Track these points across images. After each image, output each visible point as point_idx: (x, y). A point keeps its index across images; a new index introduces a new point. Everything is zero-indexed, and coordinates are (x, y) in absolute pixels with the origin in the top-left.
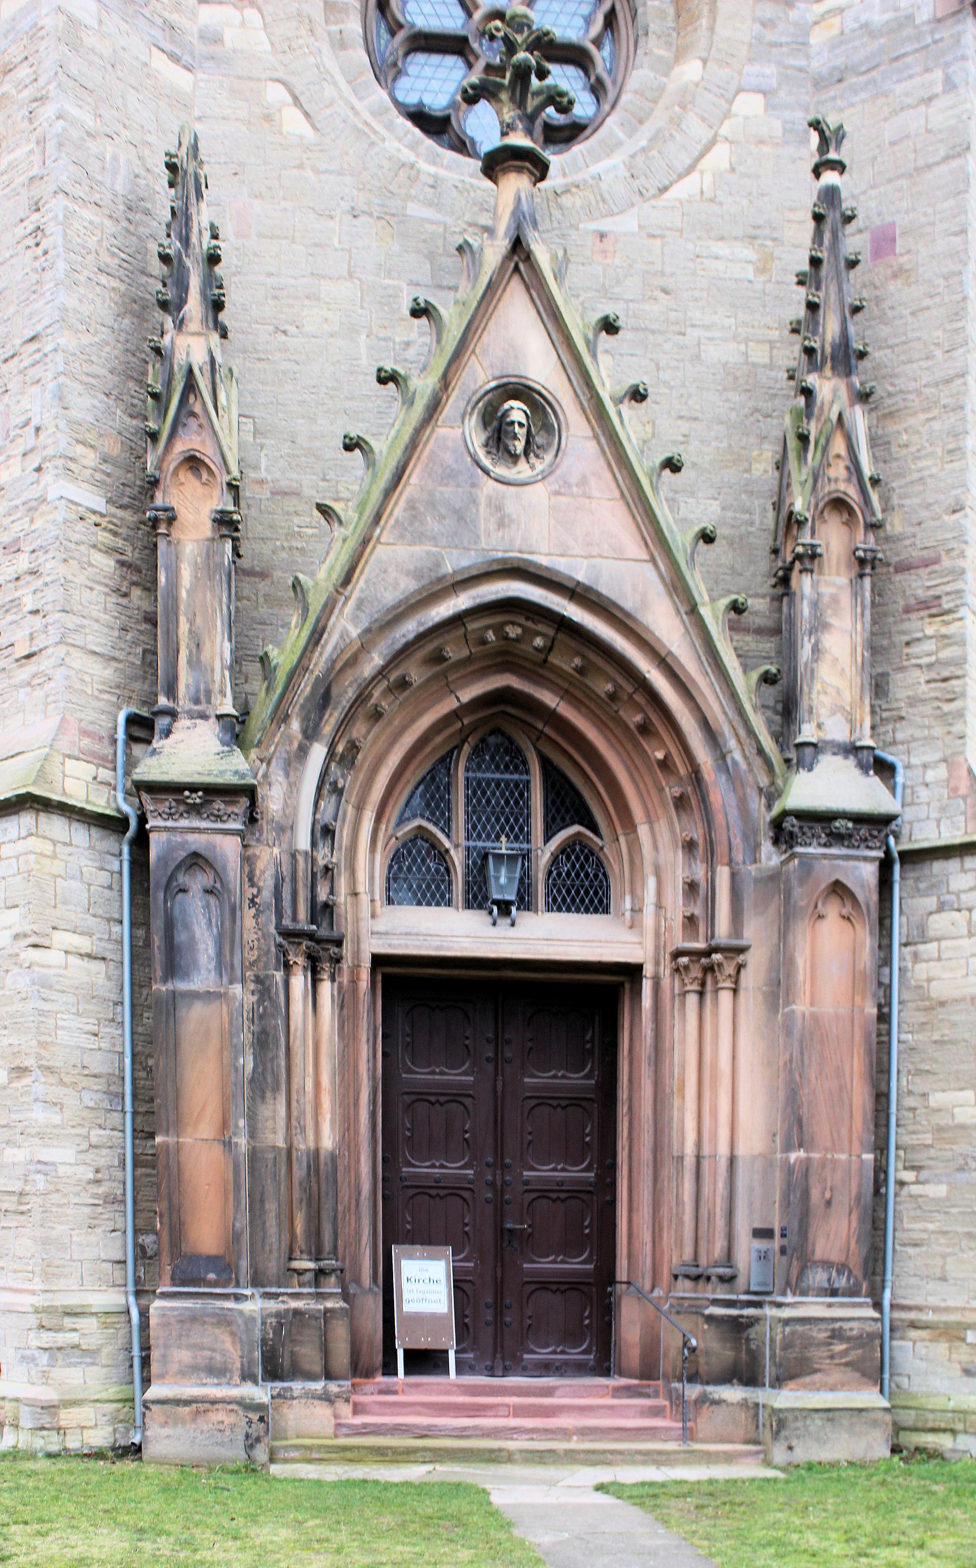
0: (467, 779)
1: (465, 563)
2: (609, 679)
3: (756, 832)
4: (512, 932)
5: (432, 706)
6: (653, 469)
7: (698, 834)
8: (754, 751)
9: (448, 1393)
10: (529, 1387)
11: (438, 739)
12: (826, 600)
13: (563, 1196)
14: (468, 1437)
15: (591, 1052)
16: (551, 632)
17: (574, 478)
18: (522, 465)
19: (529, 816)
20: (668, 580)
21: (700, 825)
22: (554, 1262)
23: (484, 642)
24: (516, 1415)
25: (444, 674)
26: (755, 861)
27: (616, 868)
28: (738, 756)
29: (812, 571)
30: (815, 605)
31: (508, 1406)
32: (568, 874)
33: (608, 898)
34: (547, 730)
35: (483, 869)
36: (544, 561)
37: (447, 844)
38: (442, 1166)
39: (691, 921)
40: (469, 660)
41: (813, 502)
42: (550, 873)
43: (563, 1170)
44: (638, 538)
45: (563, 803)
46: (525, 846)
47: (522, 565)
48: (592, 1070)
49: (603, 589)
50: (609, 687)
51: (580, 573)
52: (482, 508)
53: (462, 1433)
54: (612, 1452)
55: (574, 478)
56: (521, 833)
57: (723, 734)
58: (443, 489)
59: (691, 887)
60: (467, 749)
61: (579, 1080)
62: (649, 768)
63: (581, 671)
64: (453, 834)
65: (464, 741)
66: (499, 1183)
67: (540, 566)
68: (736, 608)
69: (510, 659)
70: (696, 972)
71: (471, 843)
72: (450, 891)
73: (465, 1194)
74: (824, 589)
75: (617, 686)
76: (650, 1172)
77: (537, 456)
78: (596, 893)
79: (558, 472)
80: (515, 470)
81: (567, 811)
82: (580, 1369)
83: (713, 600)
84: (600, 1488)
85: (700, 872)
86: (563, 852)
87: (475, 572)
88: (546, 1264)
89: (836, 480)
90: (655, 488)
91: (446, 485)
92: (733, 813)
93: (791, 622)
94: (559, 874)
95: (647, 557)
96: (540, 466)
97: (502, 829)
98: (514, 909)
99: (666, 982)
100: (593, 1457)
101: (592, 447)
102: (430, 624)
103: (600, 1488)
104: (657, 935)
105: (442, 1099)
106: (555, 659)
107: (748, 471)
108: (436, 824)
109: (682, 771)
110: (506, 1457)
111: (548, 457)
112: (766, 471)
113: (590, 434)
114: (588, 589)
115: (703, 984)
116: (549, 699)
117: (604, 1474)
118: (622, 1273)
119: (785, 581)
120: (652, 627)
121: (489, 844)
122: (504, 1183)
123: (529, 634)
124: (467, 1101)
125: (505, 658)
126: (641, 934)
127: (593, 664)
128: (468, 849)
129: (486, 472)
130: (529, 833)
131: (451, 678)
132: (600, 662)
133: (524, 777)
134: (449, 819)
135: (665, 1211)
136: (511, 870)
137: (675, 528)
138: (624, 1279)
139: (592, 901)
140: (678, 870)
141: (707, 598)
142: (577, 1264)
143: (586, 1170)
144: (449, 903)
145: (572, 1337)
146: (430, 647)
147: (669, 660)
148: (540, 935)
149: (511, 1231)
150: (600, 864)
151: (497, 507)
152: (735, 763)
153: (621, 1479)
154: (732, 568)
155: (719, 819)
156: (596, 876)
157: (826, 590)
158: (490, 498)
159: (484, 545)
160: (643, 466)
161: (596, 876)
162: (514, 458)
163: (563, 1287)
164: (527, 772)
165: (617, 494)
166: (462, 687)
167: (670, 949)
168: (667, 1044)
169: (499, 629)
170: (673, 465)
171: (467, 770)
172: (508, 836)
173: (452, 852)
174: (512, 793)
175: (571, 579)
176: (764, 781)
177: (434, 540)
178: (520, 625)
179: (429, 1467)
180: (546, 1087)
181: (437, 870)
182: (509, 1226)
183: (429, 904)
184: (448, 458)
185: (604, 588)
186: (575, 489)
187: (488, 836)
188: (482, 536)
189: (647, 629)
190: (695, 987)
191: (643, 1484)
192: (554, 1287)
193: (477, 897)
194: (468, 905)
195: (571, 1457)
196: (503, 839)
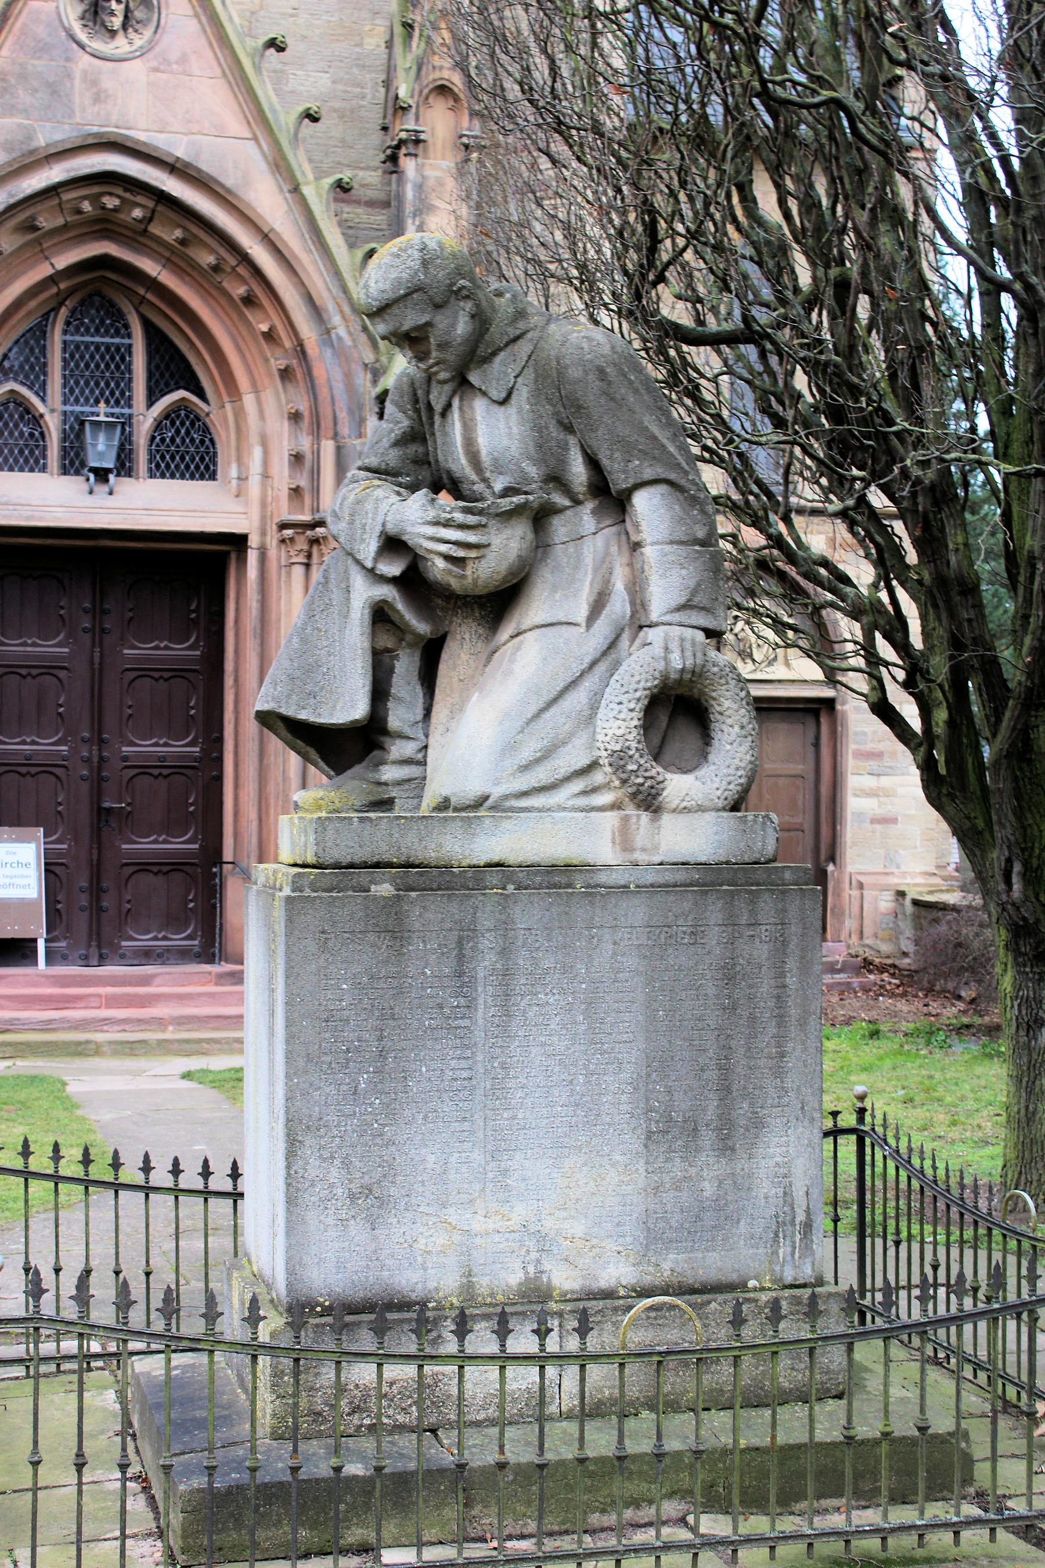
0: (65, 342)
1: (58, 137)
2: (212, 251)
3: (361, 407)
4: (110, 502)
5: (24, 273)
6: (255, 49)
7: (303, 406)
8: (360, 328)
9: (35, 985)
10: (124, 977)
11: (33, 304)
12: (431, 183)
13: (165, 772)
14: (54, 1030)
15: (195, 622)
16: (151, 204)
17: (174, 56)
18: (121, 40)
19: (130, 380)
20: (270, 158)
21: (306, 397)
22: (155, 842)
23: (79, 212)
24: (108, 1006)
25: (38, 242)
26: (360, 435)
27: (223, 433)
28: (342, 332)
29: (416, 155)
30: (420, 187)
31: (99, 996)
32: (173, 440)
33: (215, 464)
34: (149, 296)
35: (80, 435)
36: (142, 136)
37: (41, 408)
38: (34, 743)
39: (296, 492)
40: (65, 227)
41: (417, 88)
42: (153, 438)
43: (166, 745)
44: (241, 116)
45: (167, 367)
46: (126, 411)
47: (119, 140)
48: (197, 640)
49: (204, 167)
50: (211, 259)
51: (180, 149)
52: (77, 83)
53: (47, 1026)
54: (208, 1041)
55: (174, 56)
56: (122, 397)
57: (327, 311)
58: (35, 62)
59: (297, 458)
60: (63, 312)
61: (184, 651)
62: (256, 340)
63: (183, 242)
64: (49, 398)
65: (61, 304)
66: (96, 759)
67: (138, 142)
68: (342, 188)
69: (109, 226)
70: (302, 544)
71: (68, 408)
72: (45, 457)
73: (58, 771)
74: (429, 172)
75: (220, 258)
76: (256, 747)
77: (136, 31)
78: (202, 459)
79: (157, 49)
80: (113, 45)
81: (172, 376)
82: (184, 955)
83: (317, 179)
84: (187, 1076)
85: (305, 444)
86: (166, 418)
87: (69, 146)
88: (146, 845)
89: (441, 68)
90: (258, 68)
91: (39, 58)
92: (339, 388)
93: (400, 198)
94: (163, 440)
95: (249, 136)
96: (139, 41)
97: (102, 394)
98: (111, 477)
99: (273, 552)
100: (188, 1046)
101: (193, 26)
102: (21, 196)
103: (187, 1076)
104: (264, 505)
105: (34, 672)
106: (155, 229)
107: (360, 45)
108: (30, 388)
109: (288, 344)
110: (94, 1050)
111: (148, 33)
112: (378, 46)
113: (191, 12)
114: (188, 165)
115: (309, 556)
116: (150, 266)
117: (194, 1063)
118: (228, 855)
119: (393, 159)
120: (255, 204)
121: (87, 409)
122: (101, 759)
123: (127, 204)
124: (62, 674)
125: (104, 226)
126: (247, 503)
127: (195, 236)
128: (65, 413)
129: (82, 47)
130: (130, 398)
131: (45, 246)
132: (202, 234)
133: (126, 341)
134: (44, 382)
135: (271, 787)
136: (109, 439)
137: (278, 107)
138: (230, 860)
139: (197, 467)
140: (285, 439)
141: (311, 177)
142: (182, 844)
143: (191, 744)
144: (44, 469)
145: (174, 921)
146: (22, 216)
147: (271, 236)
148: (139, 504)
149: (109, 810)
150: (206, 430)
151: (92, 82)
152: (340, 338)
153: (212, 1068)
154: (343, 141)
155: (323, 393)
156: (202, 442)
157: (431, 173)
158: (85, 73)
159: (78, 120)
160: (245, 48)
161: (202, 442)
162: (113, 33)
163: (165, 869)
164: (129, 336)
165: (218, 72)
166: (59, 253)
167: (277, 520)
168: (274, 616)
169: (95, 199)
170: (275, 45)
171: (65, 332)
172: (107, 402)
173: (47, 417)
174: (113, 358)
175: (170, 154)
176: (369, 357)
177: (26, 112)
178: (118, 197)
179: (8, 1063)
180: (148, 659)
181: (31, 435)
182: (106, 805)
183: (21, 470)
184: (41, 31)
185: (205, 165)
186: (175, 66)
187: (87, 400)
188: (77, 110)
189: (249, 205)
190: (301, 559)
191: (230, 1070)
192: (155, 869)
193: (73, 462)
194: (65, 471)
195: (165, 1048)
196: (102, 405)
